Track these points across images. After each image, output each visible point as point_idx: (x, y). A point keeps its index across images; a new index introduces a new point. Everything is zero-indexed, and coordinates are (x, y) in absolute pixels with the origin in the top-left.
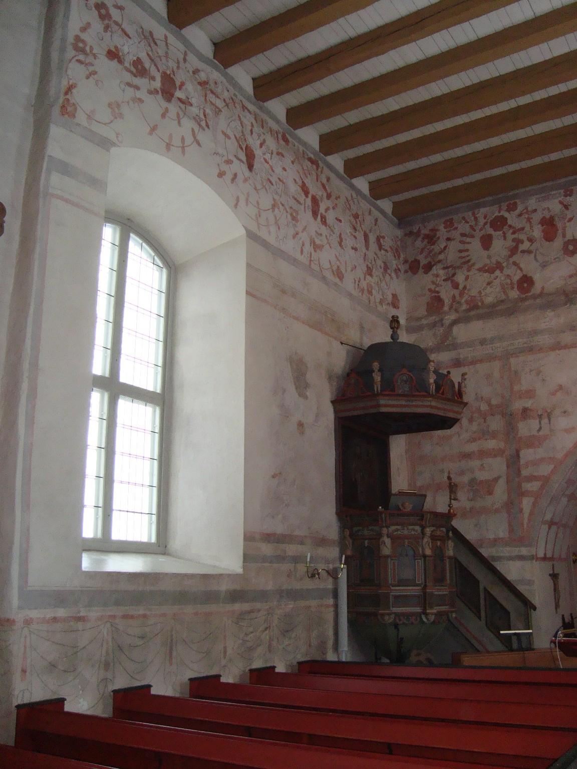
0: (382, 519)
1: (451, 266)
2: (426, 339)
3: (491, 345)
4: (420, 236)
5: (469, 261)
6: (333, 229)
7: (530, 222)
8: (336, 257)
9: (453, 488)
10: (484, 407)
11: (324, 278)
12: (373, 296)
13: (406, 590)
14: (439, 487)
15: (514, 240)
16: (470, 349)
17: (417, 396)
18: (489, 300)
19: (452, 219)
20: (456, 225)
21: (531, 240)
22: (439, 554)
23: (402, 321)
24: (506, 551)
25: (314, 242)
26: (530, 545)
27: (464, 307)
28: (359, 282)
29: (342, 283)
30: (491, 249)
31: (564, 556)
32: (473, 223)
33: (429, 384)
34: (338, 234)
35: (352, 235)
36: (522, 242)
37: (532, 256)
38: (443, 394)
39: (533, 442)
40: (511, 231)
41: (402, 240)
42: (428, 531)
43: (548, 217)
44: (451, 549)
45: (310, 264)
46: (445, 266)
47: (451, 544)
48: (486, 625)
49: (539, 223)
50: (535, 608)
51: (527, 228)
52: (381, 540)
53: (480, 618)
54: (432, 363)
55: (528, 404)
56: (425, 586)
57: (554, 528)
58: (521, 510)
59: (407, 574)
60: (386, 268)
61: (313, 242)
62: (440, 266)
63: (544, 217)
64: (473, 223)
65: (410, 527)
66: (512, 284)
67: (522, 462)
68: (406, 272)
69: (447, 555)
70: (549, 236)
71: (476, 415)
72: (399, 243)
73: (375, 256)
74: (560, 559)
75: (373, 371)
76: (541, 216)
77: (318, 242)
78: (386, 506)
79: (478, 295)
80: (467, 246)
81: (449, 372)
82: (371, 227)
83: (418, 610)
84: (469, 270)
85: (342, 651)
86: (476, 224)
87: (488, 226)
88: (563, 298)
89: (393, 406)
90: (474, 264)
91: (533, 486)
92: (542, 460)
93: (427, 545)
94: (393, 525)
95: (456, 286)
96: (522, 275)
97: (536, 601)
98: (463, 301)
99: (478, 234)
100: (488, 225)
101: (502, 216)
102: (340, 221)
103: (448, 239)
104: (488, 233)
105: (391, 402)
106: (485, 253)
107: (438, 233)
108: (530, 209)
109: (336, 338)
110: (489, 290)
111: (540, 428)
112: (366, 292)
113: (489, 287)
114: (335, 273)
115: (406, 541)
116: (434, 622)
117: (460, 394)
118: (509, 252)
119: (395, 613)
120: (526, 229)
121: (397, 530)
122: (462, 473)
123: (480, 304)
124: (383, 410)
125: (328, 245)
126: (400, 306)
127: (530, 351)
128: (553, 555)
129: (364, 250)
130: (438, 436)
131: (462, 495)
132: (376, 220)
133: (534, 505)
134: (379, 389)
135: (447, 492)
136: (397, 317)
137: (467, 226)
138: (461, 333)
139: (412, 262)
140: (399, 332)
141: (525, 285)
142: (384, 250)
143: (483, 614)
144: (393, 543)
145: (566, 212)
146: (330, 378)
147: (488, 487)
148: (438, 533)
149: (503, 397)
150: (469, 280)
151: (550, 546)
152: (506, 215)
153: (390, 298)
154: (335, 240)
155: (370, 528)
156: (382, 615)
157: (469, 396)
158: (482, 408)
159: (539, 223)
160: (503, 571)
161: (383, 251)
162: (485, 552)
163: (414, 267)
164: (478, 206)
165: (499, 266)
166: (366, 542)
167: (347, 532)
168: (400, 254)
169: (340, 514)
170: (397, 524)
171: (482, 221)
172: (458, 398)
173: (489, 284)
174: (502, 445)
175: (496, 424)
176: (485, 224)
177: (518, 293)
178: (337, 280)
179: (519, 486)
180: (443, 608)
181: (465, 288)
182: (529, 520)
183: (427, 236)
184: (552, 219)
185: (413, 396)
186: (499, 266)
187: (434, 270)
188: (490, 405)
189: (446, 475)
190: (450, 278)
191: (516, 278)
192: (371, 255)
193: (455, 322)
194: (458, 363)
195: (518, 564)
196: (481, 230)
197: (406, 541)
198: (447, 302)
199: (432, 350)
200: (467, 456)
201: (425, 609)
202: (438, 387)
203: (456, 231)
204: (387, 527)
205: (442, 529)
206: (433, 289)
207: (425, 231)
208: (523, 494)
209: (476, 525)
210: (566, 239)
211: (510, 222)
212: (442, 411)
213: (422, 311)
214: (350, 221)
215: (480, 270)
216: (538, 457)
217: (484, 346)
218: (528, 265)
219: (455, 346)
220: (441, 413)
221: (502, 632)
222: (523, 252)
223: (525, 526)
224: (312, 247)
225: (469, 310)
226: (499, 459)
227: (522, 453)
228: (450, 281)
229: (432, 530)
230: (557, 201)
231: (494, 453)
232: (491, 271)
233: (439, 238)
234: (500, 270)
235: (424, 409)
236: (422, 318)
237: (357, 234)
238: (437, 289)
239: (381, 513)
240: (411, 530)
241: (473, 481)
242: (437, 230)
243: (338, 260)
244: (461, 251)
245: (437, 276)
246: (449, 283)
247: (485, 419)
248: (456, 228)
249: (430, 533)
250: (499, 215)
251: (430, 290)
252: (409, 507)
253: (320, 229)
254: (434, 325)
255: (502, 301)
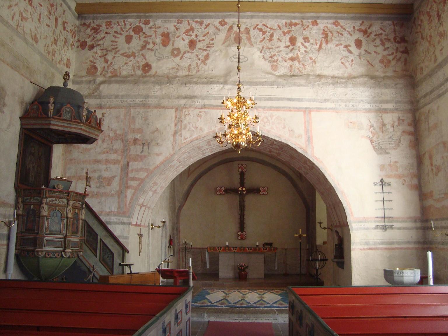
0: (43, 192)
1: (106, 49)
2: (83, 90)
3: (121, 100)
4: (89, 27)
5: (116, 48)
6: (36, 9)
7: (156, 34)
8: (36, 28)
9: (88, 179)
10: (112, 135)
11: (25, 39)
12: (55, 58)
13: (56, 237)
14: (79, 178)
15: (144, 41)
16: (109, 100)
17: (75, 122)
18: (124, 73)
19: (111, 21)
20: (112, 26)
21: (154, 44)
22: (76, 217)
23: (71, 76)
24: (114, 219)
25: (22, 15)
26: (129, 217)
27: (109, 75)
28: (48, 47)
29: (37, 45)
30: (130, 44)
31: (147, 224)
32: (123, 27)
33: (83, 116)
34: (39, 14)
35: (48, 16)
36: (149, 43)
37: (153, 53)
38: (90, 123)
39: (136, 158)
40: (144, 36)
41: (78, 28)
42: (71, 202)
43: (166, 32)
44: (83, 215)
45: (17, 29)
46: (102, 48)
47: (84, 212)
48: (100, 261)
49: (161, 35)
50: (128, 252)
51: (154, 36)
52: (41, 206)
53: (96, 256)
54: (86, 104)
55: (138, 136)
56: (66, 235)
57: (143, 208)
58: (126, 197)
59: (56, 228)
60: (66, 42)
61: (21, 14)
62: (99, 47)
63: (164, 32)
64: (123, 27)
65: (60, 200)
66: (139, 67)
67: (130, 169)
68: (78, 47)
69: (80, 218)
70: (165, 43)
71: (107, 139)
72: (76, 29)
73: (60, 34)
74: (145, 226)
75: (49, 103)
76: (163, 31)
77: (24, 15)
78: (47, 185)
79: (118, 69)
80: (117, 39)
81: (95, 111)
82: (61, 15)
83: (61, 249)
84: (115, 54)
85: (9, 273)
86: (125, 28)
87: (131, 30)
88: (166, 79)
89: (60, 126)
90: (119, 51)
91: (134, 184)
92: (141, 169)
93: (70, 211)
94: (50, 197)
95: (106, 61)
96: (145, 62)
97: (129, 248)
98: (109, 71)
99: (125, 34)
100: (132, 29)
101: (140, 26)
102: (41, 6)
103: (106, 33)
104: (130, 34)
105: (57, 123)
106: (127, 46)
107: (101, 28)
108: (157, 26)
109: (27, 78)
110: (125, 67)
111: (143, 151)
112: (51, 54)
113: (125, 66)
114: (33, 38)
115: (57, 208)
116: (69, 257)
117: (100, 124)
118: (141, 48)
119: (46, 251)
120: (152, 37)
121: (52, 201)
122: (94, 171)
123: (118, 74)
124: (52, 127)
125: (31, 18)
126: (71, 67)
127: (143, 106)
128: (141, 224)
129: (54, 27)
130: (83, 148)
131: (93, 184)
132: (64, 11)
133: (134, 194)
134: (52, 114)
135: (85, 182)
136: (69, 73)
137: (119, 27)
138: (105, 89)
139: (82, 42)
140: (68, 82)
141: (147, 68)
142: (66, 30)
143: (98, 255)
144: (49, 208)
145: (177, 32)
146: (22, 103)
147: (109, 181)
148: (77, 205)
149: (124, 130)
150: (115, 59)
151: (140, 219)
152: (143, 26)
153: (65, 61)
154: (36, 17)
155: (36, 198)
156: (38, 252)
157: (104, 127)
158: (111, 135)
159: (161, 35)
160: (112, 230)
161: (65, 32)
162: (103, 218)
163: (83, 45)
164: (127, 17)
165: (133, 55)
166: (32, 207)
167: (20, 200)
168: (75, 35)
169: (16, 188)
170: (52, 197)
171: (128, 27)
172: (98, 127)
173: (126, 64)
174: (119, 158)
175: (118, 145)
176: (131, 28)
177: (142, 72)
178: (34, 43)
179: (127, 183)
180: (77, 249)
181: (111, 63)
182: (130, 203)
183: (94, 28)
184: (168, 34)
185: (71, 121)
186: (133, 55)
187: (95, 50)
188: (115, 133)
189: (85, 172)
190: (104, 56)
191: (142, 64)
192: (57, 32)
193: (103, 82)
194: (100, 107)
195: (121, 227)
196: (127, 31)
197: (57, 208)
198: (100, 69)
199: (86, 97)
200: (98, 162)
201: (65, 249)
202: (88, 118)
203: (112, 29)
204: (46, 198)
205: (79, 202)
206: (92, 61)
207: (93, 25)
208: (128, 187)
209: (99, 203)
210: (174, 47)
211: (144, 30)
212: (88, 133)
213: (84, 73)
214: (48, 7)
215: (122, 54)
216: (139, 167)
217: (117, 100)
218: (151, 57)
219: (100, 97)
220: (87, 134)
221: (430, 254)
222: (149, 49)
223: (127, 205)
224: (20, 17)
225: (111, 77)
226: (116, 166)
227: (130, 164)
228: (103, 57)
229: (73, 202)
230: (172, 25)
231: (115, 162)
232: (128, 56)
233: (101, 31)
234: (134, 57)
235: (76, 130)
236: (83, 77)
237: (51, 17)
238: (95, 61)
239: (43, 189)
240: (61, 201)
241: (100, 177)
242: (101, 26)
243: (36, 30)
244: (112, 41)
245: (96, 53)
246: (103, 59)
247: (111, 141)
248: (112, 28)
249: (72, 204)
250: (139, 25)
251: (91, 61)
252: (61, 187)
253: (27, 7)
254: (90, 82)
255: (132, 75)
